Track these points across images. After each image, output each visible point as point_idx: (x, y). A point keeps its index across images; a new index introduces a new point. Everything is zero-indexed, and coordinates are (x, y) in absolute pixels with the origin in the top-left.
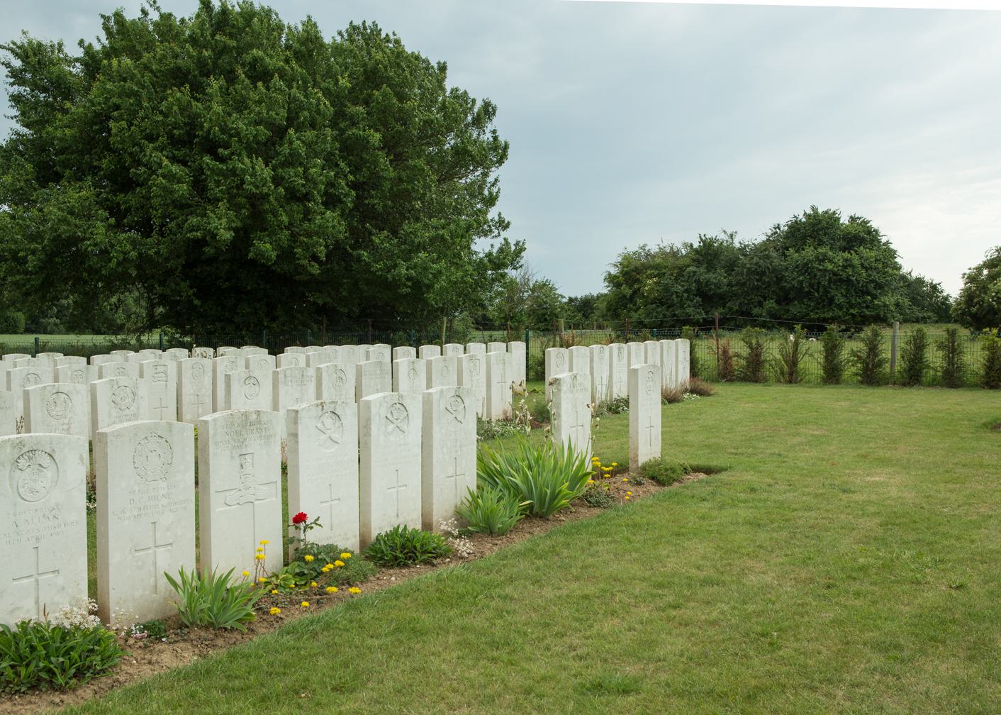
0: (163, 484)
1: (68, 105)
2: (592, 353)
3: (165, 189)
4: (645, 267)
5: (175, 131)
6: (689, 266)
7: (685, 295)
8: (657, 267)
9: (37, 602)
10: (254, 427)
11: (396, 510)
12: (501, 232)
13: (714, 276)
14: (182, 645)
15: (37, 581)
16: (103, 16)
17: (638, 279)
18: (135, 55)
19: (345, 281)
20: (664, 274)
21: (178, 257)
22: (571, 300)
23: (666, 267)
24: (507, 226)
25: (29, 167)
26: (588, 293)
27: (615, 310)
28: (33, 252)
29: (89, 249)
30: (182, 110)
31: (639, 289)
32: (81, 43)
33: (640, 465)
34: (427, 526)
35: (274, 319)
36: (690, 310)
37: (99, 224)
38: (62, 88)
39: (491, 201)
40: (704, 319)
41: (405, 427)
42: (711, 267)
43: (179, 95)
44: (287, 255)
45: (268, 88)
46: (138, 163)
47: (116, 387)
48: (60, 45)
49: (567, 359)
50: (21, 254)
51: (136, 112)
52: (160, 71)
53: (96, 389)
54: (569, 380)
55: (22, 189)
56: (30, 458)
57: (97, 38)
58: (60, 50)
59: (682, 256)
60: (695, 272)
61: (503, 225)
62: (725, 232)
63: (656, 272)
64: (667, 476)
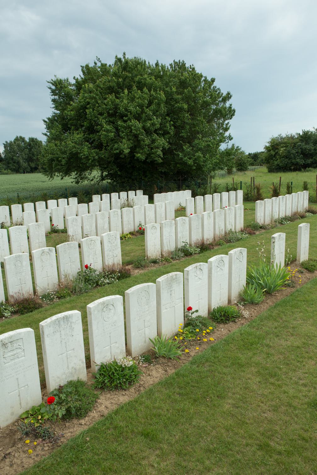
0: (147, 307)
1: (72, 103)
2: (272, 201)
3: (106, 135)
4: (281, 143)
5: (110, 111)
6: (298, 142)
7: (296, 154)
8: (285, 143)
9: (111, 353)
10: (175, 280)
11: (219, 299)
12: (229, 141)
13: (308, 146)
14: (157, 366)
15: (111, 346)
16: (81, 66)
17: (278, 148)
18: (94, 81)
19: (172, 163)
20: (288, 146)
21: (112, 157)
22: (250, 154)
23: (289, 143)
24: (232, 139)
25: (60, 126)
26: (256, 151)
27: (268, 160)
28: (64, 158)
29: (82, 157)
30: (112, 103)
31: (278, 152)
32: (74, 78)
33: (301, 262)
34: (229, 301)
35: (146, 177)
36: (298, 160)
37: (86, 147)
38: (68, 97)
39: (226, 129)
40: (304, 164)
41: (223, 268)
42: (307, 143)
43: (112, 97)
44: (148, 155)
45: (142, 93)
46: (98, 125)
47: (109, 236)
48: (67, 79)
49: (263, 205)
50: (60, 159)
51: (95, 105)
52: (104, 88)
53: (103, 238)
54: (278, 237)
55: (58, 135)
56: (107, 307)
57: (79, 75)
58: (67, 81)
59: (296, 138)
60: (300, 145)
61: (230, 138)
62: (314, 128)
63: (285, 145)
64: (312, 268)
